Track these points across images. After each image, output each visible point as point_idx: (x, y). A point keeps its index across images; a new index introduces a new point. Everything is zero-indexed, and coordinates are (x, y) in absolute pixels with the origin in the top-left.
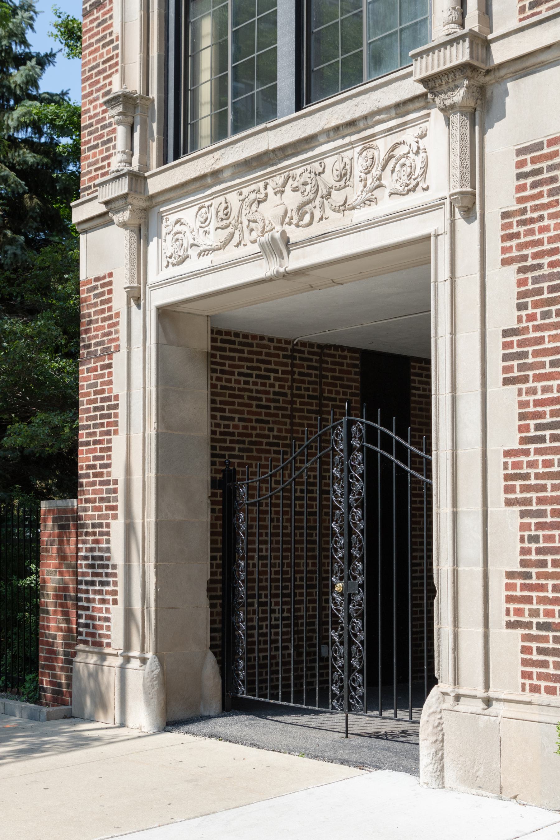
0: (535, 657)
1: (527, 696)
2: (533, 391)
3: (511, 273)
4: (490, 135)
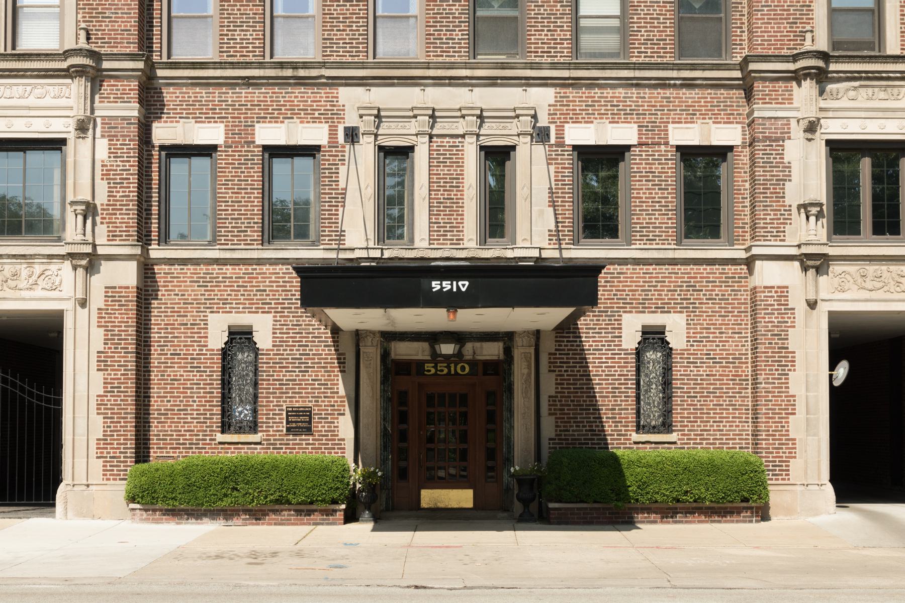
0: (109, 468)
2: (110, 375)
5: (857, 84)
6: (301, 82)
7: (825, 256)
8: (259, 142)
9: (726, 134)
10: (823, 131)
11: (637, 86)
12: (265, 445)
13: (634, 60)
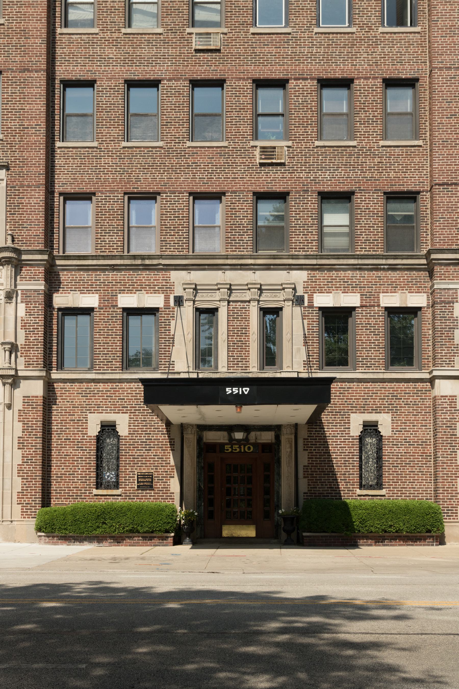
0: (25, 510)
1: (22, 519)
3: (21, 424)
4: (15, 390)
6: (147, 268)
8: (382, 305)
9: (417, 300)
11: (360, 269)
12: (125, 495)
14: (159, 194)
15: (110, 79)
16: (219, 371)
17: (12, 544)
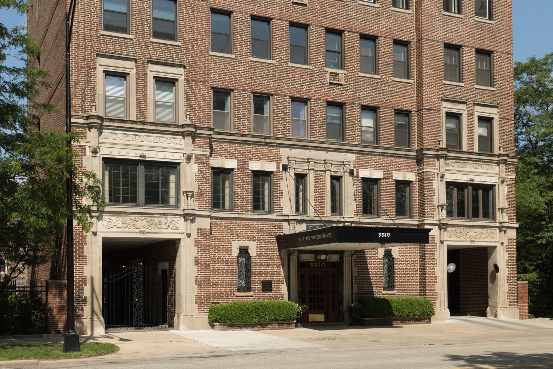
5: (454, 161)
6: (267, 144)
7: (194, 215)
8: (394, 178)
9: (411, 177)
10: (100, 153)
11: (383, 155)
12: (255, 296)
13: (381, 145)
14: (272, 95)
15: (242, 13)
16: (309, 215)
17: (193, 331)
